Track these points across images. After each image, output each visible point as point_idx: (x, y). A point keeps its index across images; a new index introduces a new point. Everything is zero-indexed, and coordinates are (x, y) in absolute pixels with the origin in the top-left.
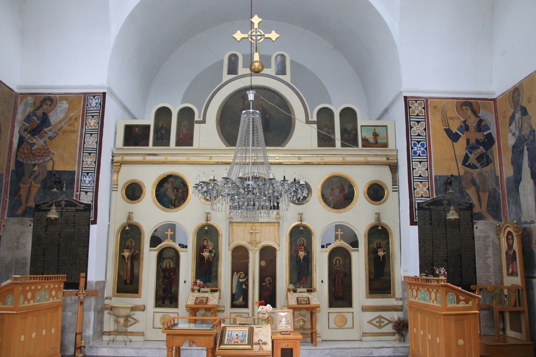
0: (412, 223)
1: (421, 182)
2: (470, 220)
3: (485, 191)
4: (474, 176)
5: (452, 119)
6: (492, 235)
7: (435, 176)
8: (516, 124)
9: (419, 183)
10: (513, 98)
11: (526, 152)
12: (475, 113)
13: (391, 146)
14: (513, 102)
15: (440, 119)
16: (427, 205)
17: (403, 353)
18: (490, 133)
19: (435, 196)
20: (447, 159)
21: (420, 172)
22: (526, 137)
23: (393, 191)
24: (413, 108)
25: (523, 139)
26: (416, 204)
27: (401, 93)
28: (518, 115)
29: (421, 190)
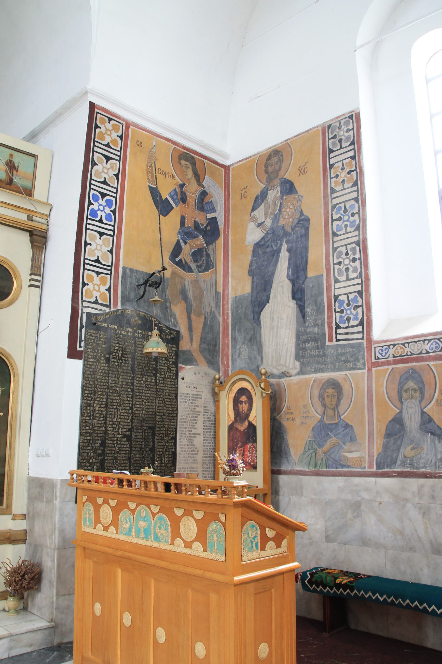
0: (73, 354)
1: (98, 273)
2: (174, 363)
3: (199, 315)
4: (186, 283)
5: (164, 174)
6: (206, 395)
7: (124, 268)
8: (267, 208)
9: (94, 275)
10: (266, 166)
11: (284, 255)
12: (198, 178)
13: (38, 194)
14: (266, 172)
15: (144, 165)
16: (105, 321)
17: (31, 645)
18: (215, 218)
19: (119, 307)
20: (146, 240)
21: (98, 254)
22: (289, 230)
23: (31, 286)
24: (103, 129)
25: (281, 233)
26: (84, 316)
27: (86, 93)
28: (273, 194)
29: (96, 288)
